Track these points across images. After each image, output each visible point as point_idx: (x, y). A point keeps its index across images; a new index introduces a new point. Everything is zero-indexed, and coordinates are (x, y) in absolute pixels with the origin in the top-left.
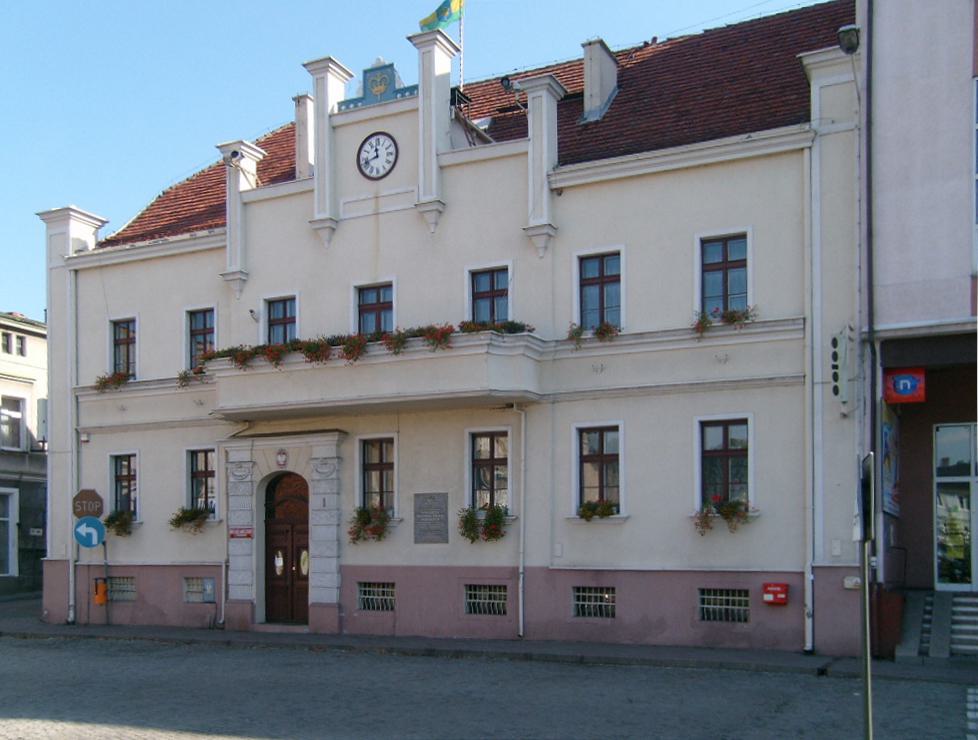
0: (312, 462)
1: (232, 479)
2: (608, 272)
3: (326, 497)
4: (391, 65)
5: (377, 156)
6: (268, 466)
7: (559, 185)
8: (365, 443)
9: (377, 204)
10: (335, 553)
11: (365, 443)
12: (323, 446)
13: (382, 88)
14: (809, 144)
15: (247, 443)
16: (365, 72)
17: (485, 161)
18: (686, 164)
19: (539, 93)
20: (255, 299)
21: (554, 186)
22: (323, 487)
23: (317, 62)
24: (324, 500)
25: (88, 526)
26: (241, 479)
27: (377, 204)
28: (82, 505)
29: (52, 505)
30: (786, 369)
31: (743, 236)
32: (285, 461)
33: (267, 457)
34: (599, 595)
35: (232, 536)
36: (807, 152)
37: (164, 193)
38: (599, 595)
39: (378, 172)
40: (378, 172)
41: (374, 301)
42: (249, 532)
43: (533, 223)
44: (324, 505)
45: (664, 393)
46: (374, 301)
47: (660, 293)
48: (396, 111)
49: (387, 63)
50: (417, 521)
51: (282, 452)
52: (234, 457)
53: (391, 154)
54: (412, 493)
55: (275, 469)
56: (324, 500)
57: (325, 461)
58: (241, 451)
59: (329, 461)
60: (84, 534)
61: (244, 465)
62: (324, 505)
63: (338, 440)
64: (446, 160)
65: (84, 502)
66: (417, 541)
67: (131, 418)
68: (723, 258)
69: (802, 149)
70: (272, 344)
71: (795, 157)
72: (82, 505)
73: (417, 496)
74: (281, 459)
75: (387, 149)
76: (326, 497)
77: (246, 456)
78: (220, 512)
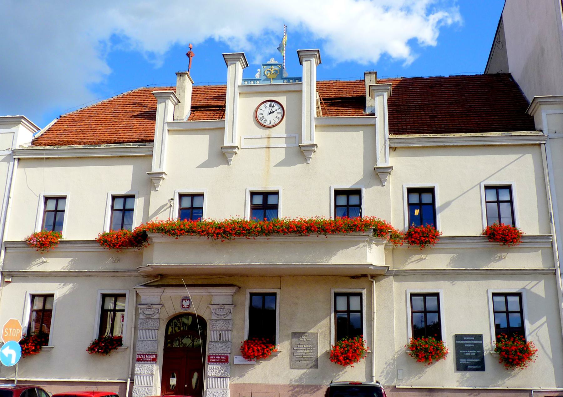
0: (212, 307)
1: (141, 316)
2: (127, 207)
3: (222, 332)
8: (252, 295)
9: (269, 142)
11: (252, 295)
12: (221, 295)
14: (544, 142)
15: (158, 291)
17: (351, 126)
18: (456, 144)
22: (220, 325)
24: (220, 335)
25: (10, 348)
26: (149, 318)
27: (269, 142)
28: (8, 331)
30: (539, 265)
31: (201, 195)
32: (189, 305)
33: (172, 301)
35: (139, 360)
36: (543, 146)
39: (270, 122)
40: (270, 122)
41: (265, 203)
42: (154, 357)
44: (220, 339)
46: (265, 203)
48: (285, 90)
51: (186, 298)
52: (144, 299)
55: (179, 310)
56: (220, 335)
57: (222, 306)
58: (152, 295)
59: (226, 307)
60: (7, 356)
61: (154, 307)
62: (220, 339)
65: (11, 329)
66: (291, 368)
69: (540, 144)
71: (536, 148)
72: (8, 331)
74: (186, 303)
76: (222, 332)
77: (156, 300)
78: (127, 341)
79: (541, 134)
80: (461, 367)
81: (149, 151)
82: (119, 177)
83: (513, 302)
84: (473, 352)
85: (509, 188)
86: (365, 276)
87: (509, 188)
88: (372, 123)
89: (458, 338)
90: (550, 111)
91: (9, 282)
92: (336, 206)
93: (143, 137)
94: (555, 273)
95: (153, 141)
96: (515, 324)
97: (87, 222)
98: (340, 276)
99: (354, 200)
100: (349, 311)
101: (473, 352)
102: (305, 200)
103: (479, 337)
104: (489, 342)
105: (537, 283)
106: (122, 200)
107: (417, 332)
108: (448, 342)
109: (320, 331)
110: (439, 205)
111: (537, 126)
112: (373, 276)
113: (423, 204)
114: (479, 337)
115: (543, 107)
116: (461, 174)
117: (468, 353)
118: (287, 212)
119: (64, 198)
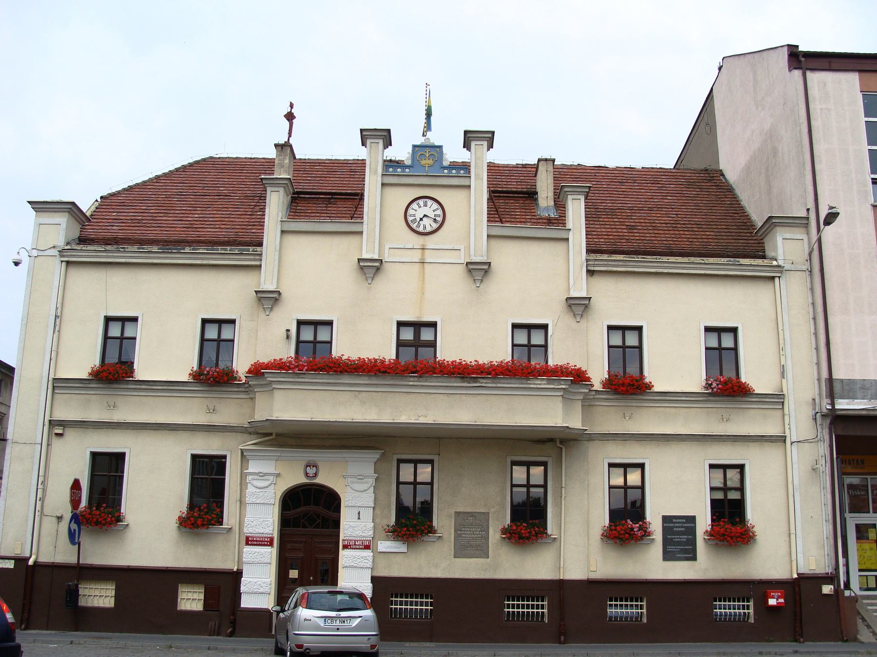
3: (361, 510)
4: (440, 147)
5: (425, 216)
6: (295, 478)
7: (592, 268)
9: (423, 255)
10: (370, 564)
13: (430, 162)
16: (414, 146)
18: (199, 262)
19: (578, 197)
20: (285, 319)
21: (590, 268)
23: (375, 130)
27: (423, 255)
29: (389, 506)
34: (746, 603)
36: (777, 280)
37: (102, 197)
38: (746, 603)
39: (425, 227)
41: (416, 335)
43: (574, 294)
45: (766, 441)
46: (416, 335)
47: (675, 364)
49: (437, 144)
50: (457, 537)
53: (439, 216)
54: (452, 511)
63: (378, 460)
64: (287, 227)
67: (117, 416)
68: (722, 346)
69: (773, 278)
70: (318, 359)
73: (458, 514)
74: (311, 471)
75: (420, 207)
76: (361, 510)
79: (775, 263)
80: (668, 556)
81: (255, 260)
82: (220, 292)
83: (733, 474)
84: (684, 538)
85: (734, 330)
86: (551, 440)
87: (734, 330)
88: (467, 184)
89: (666, 519)
90: (788, 236)
91: (60, 435)
92: (514, 345)
93: (232, 235)
94: (785, 441)
95: (260, 244)
96: (733, 495)
97: (166, 354)
98: (519, 440)
99: (537, 338)
100: (528, 486)
101: (684, 538)
102: (474, 335)
103: (692, 519)
104: (704, 523)
105: (863, 619)
106: (216, 326)
107: (615, 515)
108: (654, 518)
109: (493, 510)
110: (742, 161)
111: (769, 253)
112: (563, 441)
113: (626, 344)
114: (692, 519)
115: (778, 229)
116: (674, 317)
117: (677, 538)
118: (449, 350)
119: (135, 320)
